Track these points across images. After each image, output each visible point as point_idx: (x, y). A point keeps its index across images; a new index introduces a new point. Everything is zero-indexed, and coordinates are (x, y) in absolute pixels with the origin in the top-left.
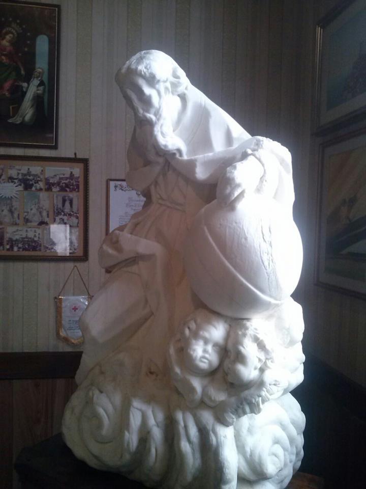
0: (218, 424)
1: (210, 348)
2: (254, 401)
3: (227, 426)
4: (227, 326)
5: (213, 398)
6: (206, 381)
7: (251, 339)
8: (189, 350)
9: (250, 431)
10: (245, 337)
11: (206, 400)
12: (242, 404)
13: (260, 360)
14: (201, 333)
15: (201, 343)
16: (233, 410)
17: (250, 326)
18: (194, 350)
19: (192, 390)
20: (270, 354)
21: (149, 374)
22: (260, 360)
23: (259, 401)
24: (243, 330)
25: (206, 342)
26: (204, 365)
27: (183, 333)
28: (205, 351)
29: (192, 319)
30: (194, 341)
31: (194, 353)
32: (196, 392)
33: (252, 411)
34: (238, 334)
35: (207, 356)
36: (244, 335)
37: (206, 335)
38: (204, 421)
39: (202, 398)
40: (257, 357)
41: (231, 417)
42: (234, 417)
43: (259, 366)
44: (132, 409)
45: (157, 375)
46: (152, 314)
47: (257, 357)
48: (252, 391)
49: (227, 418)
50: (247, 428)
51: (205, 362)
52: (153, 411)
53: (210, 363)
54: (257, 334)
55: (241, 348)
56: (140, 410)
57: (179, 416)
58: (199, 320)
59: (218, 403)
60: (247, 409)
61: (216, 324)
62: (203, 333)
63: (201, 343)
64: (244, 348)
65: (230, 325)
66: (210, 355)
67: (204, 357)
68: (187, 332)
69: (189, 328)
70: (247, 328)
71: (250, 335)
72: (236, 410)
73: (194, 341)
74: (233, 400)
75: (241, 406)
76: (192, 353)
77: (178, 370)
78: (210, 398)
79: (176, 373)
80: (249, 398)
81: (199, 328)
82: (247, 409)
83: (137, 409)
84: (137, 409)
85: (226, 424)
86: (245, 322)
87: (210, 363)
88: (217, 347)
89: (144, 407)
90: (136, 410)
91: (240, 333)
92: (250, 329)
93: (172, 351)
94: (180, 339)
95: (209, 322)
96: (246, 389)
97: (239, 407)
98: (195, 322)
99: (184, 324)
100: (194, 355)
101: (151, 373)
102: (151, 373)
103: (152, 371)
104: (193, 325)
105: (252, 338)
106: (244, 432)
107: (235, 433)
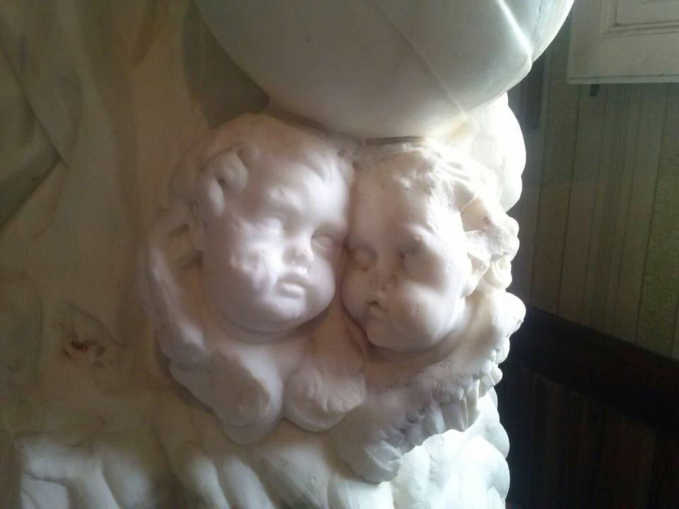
0: (347, 483)
1: (304, 242)
2: (461, 394)
3: (375, 483)
4: (347, 167)
5: (325, 408)
6: (291, 355)
7: (446, 201)
8: (233, 262)
9: (436, 478)
10: (430, 194)
11: (301, 415)
12: (425, 409)
13: (476, 264)
14: (274, 194)
15: (274, 229)
16: (396, 432)
17: (435, 158)
18: (255, 258)
19: (250, 390)
20: (504, 242)
21: (70, 350)
22: (476, 264)
23: (474, 391)
24: (414, 174)
25: (291, 222)
26: (291, 306)
27: (198, 202)
28: (292, 256)
29: (229, 150)
30: (247, 228)
31: (255, 267)
32: (265, 396)
33: (453, 423)
34: (397, 189)
35: (301, 271)
36: (425, 188)
37: (294, 199)
38: (300, 483)
39: (284, 408)
40: (469, 256)
41: (384, 453)
42: (396, 451)
43: (473, 282)
44: (26, 482)
45: (101, 351)
46: (57, 159)
47: (469, 256)
48: (458, 363)
49: (374, 458)
50: (427, 474)
51: (293, 295)
52: (108, 476)
53: (311, 293)
54: (464, 182)
55: (420, 231)
56: (62, 481)
57: (208, 478)
58: (256, 154)
59: (340, 418)
60: (439, 420)
61: (317, 158)
62: (282, 194)
63: (274, 229)
64: (429, 229)
65: (356, 166)
66: (309, 268)
67: (292, 278)
68: (217, 195)
69: (222, 182)
70: (426, 166)
71: (445, 185)
72: (404, 431)
73: (247, 228)
74: (394, 401)
75: (422, 417)
76: (246, 267)
77: (193, 335)
78: (316, 410)
79: (191, 348)
80: (450, 388)
81: (261, 177)
82: (439, 420)
83: (48, 479)
84: (48, 479)
85: (367, 475)
86: (406, 148)
87: (311, 293)
88: (326, 240)
89: (72, 468)
90: (42, 482)
91: (407, 183)
92: (437, 168)
93: (161, 270)
94: (185, 228)
95: (295, 155)
96: (433, 361)
97: (412, 421)
98: (243, 155)
99: (202, 169)
100: (258, 274)
101: (79, 346)
102: (79, 346)
103: (81, 339)
104: (238, 172)
105: (449, 195)
106: (421, 481)
107: (394, 495)
